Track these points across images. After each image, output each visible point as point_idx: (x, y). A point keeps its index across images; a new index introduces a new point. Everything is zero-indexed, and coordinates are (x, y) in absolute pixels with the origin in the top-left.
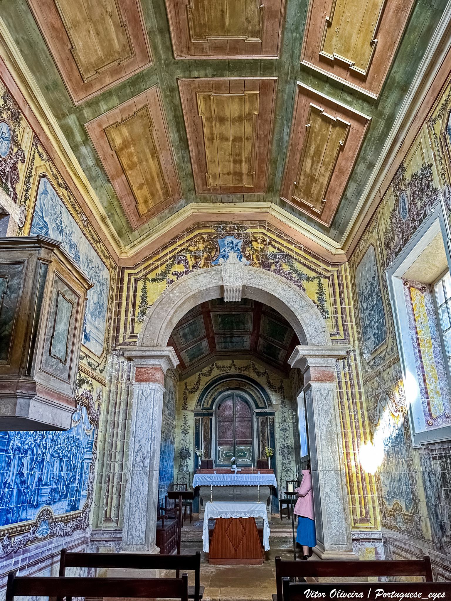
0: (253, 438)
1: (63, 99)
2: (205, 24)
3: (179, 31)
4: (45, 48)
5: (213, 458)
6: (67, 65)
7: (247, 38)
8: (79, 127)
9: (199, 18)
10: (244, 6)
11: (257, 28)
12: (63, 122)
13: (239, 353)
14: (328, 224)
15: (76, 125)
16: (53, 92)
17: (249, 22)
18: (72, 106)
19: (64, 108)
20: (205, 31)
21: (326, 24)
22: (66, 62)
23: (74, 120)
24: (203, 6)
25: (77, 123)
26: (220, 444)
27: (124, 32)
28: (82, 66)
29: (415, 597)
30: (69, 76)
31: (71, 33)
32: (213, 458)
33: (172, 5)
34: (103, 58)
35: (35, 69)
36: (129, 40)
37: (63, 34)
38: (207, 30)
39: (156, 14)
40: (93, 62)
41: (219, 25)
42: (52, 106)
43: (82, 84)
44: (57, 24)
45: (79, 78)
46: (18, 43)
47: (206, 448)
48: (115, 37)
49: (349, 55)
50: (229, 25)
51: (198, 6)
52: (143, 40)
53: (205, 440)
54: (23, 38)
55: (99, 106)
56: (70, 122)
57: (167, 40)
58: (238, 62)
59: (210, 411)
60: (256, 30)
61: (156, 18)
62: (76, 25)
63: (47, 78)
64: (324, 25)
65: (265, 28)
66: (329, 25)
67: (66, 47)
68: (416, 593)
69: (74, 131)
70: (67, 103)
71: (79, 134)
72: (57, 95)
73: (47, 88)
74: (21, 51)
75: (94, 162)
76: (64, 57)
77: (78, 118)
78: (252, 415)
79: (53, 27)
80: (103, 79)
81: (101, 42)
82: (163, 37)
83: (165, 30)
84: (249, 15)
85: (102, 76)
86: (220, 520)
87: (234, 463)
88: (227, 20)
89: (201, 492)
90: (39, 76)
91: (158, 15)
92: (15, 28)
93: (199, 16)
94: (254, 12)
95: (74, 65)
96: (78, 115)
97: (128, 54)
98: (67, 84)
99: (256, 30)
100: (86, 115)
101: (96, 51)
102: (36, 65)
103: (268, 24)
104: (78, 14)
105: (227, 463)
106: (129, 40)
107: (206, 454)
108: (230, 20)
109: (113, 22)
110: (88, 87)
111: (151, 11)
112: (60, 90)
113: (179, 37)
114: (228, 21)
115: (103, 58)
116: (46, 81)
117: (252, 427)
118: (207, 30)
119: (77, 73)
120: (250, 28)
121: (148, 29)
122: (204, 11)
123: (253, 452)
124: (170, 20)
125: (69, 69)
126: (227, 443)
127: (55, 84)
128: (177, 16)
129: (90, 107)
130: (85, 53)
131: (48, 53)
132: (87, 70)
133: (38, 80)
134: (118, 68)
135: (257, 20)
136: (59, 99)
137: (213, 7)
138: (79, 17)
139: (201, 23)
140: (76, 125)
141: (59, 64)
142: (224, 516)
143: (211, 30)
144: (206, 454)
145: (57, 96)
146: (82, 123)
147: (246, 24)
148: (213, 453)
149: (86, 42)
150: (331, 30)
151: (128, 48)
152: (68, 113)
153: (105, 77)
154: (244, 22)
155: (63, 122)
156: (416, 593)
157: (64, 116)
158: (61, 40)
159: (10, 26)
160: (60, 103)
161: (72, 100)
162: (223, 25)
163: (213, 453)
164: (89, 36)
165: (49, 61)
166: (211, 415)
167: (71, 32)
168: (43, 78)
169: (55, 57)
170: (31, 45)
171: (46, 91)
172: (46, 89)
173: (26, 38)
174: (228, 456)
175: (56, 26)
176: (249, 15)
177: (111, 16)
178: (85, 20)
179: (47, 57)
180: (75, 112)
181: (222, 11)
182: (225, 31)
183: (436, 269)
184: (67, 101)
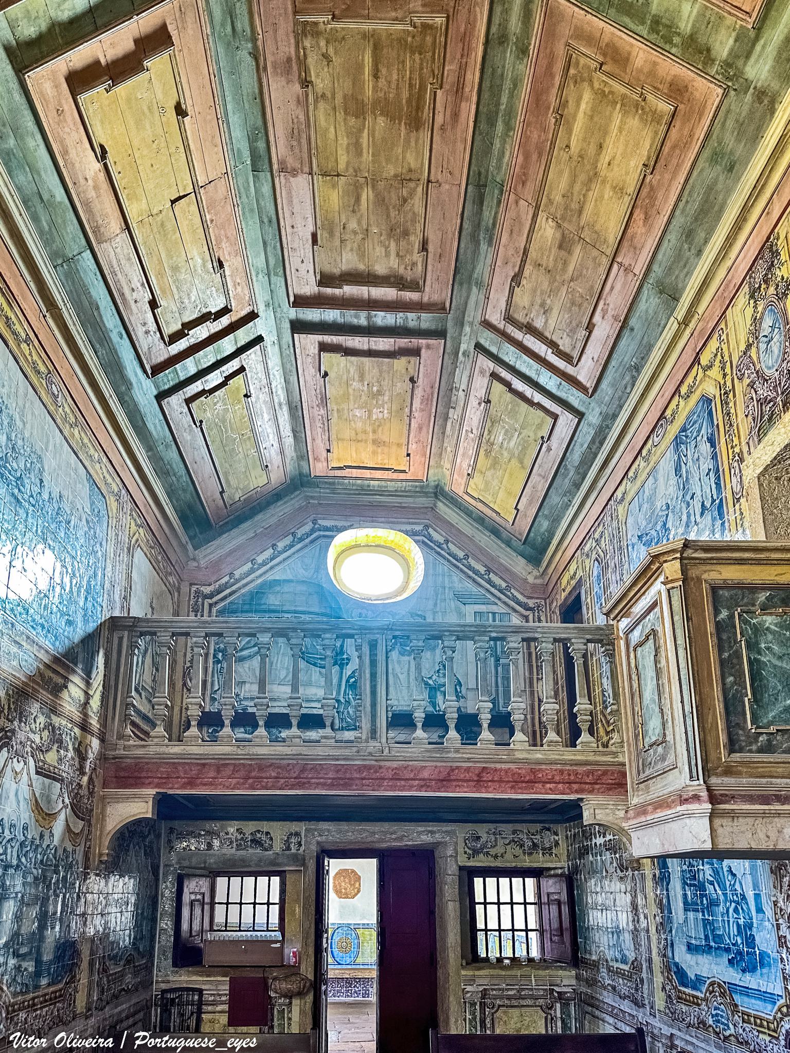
1: (730, 124)
2: (413, 53)
3: (465, 39)
4: (678, 213)
6: (674, 161)
7: (328, 23)
8: (765, 36)
9: (421, 64)
10: (336, 85)
11: (307, 43)
12: (775, 85)
14: (341, 916)
15: (764, 47)
16: (731, 153)
17: (325, 56)
18: (732, 93)
19: (746, 108)
20: (413, 37)
21: (184, 107)
22: (671, 167)
23: (757, 61)
24: (411, 85)
25: (758, 48)
27: (563, 104)
28: (656, 133)
29: (204, 1046)
30: (687, 145)
31: (632, 189)
33: (467, 90)
34: (619, 106)
35: (716, 208)
36: (562, 88)
37: (644, 200)
38: (410, 39)
39: (502, 75)
40: (637, 117)
41: (385, 51)
42: (756, 138)
43: (681, 107)
44: (639, 215)
45: (677, 123)
46: (699, 253)
48: (580, 115)
50: (365, 48)
51: (420, 87)
52: (541, 55)
54: (690, 249)
55: (693, 26)
56: (767, 67)
57: (496, 20)
60: (309, 37)
61: (504, 67)
62: (619, 190)
63: (715, 182)
64: (188, 105)
65: (292, 41)
66: (180, 111)
67: (654, 182)
68: (206, 1040)
69: (782, 37)
70: (733, 107)
71: (781, 16)
72: (730, 140)
73: (731, 169)
74: (706, 241)
76: (667, 176)
77: (748, 56)
79: (646, 219)
80: (646, 70)
81: (605, 132)
82: (504, 26)
83: (495, 40)
84: (326, 69)
85: (642, 78)
88: (368, 59)
90: (722, 193)
91: (499, 71)
92: (685, 266)
93: (421, 69)
94: (317, 76)
95: (666, 149)
96: (740, 63)
97: (577, 63)
98: (700, 141)
99: (309, 37)
100: (731, 41)
101: (621, 130)
102: (708, 212)
103: (287, 49)
104: (606, 197)
106: (562, 88)
108: (363, 60)
109: (571, 135)
110: (677, 91)
111: (507, 84)
112: (720, 144)
113: (471, 24)
114: (366, 58)
115: (619, 106)
116: (721, 178)
118: (410, 39)
119: (674, 133)
120: (323, 43)
121: (525, 61)
122: (410, 78)
124: (478, 66)
125: (678, 152)
127: (715, 158)
128: (463, 69)
129: (708, 50)
130: (637, 145)
131: (681, 205)
132: (656, 117)
133: (729, 191)
134: (608, 59)
135: (309, 60)
136: (736, 133)
137: (393, 86)
138: (608, 193)
139: (420, 54)
140: (764, 47)
141: (681, 178)
143: (401, 42)
145: (733, 139)
146: (752, 34)
147: (331, 51)
149: (624, 155)
150: (173, 103)
151: (572, 71)
152: (751, 90)
153: (640, 71)
154: (335, 53)
155: (775, 85)
156: (206, 1040)
157: (760, 94)
158: (652, 196)
159: (688, 273)
160: (740, 126)
161: (719, 108)
162: (377, 48)
164: (614, 158)
165: (690, 194)
167: (631, 189)
168: (720, 186)
169: (678, 192)
170: (689, 235)
171: (737, 165)
172: (733, 168)
173: (686, 246)
175: (642, 216)
176: (326, 69)
177: (568, 146)
178: (603, 182)
179: (687, 202)
180: (739, 74)
181: (376, 76)
182: (372, 36)
183: (375, 967)
184: (728, 111)
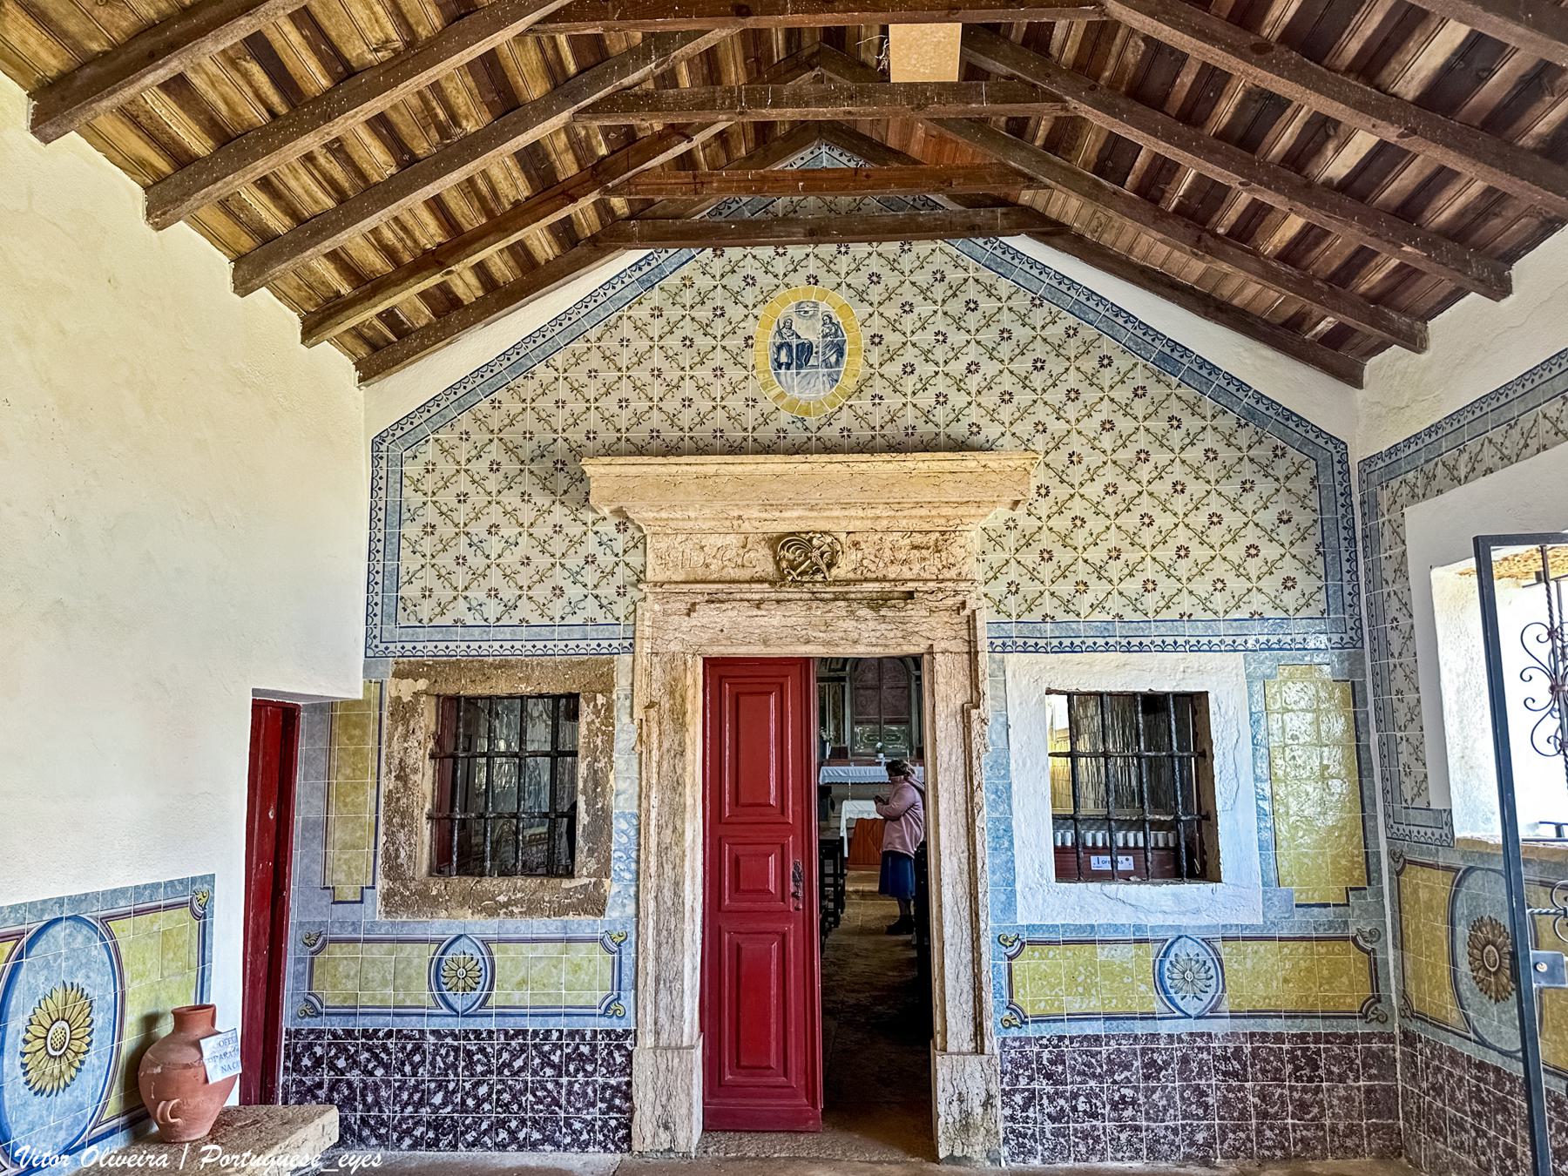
0: (910, 714)
5: (848, 743)
13: (550, 52)
26: (859, 723)
32: (848, 743)
47: (837, 729)
49: (1131, 57)
53: (835, 717)
58: (249, 1041)
59: (841, 674)
75: (368, 349)
78: (909, 680)
86: (860, 821)
87: (879, 751)
89: (834, 791)
105: (869, 750)
107: (838, 738)
117: (910, 697)
123: (910, 734)
126: (869, 722)
142: (865, 816)
144: (838, 738)
148: (848, 737)
163: (848, 737)
166: (843, 679)
174: (871, 741)
